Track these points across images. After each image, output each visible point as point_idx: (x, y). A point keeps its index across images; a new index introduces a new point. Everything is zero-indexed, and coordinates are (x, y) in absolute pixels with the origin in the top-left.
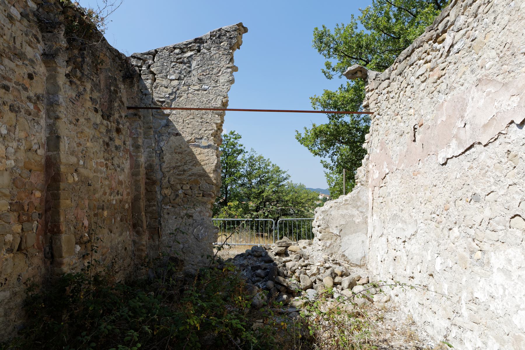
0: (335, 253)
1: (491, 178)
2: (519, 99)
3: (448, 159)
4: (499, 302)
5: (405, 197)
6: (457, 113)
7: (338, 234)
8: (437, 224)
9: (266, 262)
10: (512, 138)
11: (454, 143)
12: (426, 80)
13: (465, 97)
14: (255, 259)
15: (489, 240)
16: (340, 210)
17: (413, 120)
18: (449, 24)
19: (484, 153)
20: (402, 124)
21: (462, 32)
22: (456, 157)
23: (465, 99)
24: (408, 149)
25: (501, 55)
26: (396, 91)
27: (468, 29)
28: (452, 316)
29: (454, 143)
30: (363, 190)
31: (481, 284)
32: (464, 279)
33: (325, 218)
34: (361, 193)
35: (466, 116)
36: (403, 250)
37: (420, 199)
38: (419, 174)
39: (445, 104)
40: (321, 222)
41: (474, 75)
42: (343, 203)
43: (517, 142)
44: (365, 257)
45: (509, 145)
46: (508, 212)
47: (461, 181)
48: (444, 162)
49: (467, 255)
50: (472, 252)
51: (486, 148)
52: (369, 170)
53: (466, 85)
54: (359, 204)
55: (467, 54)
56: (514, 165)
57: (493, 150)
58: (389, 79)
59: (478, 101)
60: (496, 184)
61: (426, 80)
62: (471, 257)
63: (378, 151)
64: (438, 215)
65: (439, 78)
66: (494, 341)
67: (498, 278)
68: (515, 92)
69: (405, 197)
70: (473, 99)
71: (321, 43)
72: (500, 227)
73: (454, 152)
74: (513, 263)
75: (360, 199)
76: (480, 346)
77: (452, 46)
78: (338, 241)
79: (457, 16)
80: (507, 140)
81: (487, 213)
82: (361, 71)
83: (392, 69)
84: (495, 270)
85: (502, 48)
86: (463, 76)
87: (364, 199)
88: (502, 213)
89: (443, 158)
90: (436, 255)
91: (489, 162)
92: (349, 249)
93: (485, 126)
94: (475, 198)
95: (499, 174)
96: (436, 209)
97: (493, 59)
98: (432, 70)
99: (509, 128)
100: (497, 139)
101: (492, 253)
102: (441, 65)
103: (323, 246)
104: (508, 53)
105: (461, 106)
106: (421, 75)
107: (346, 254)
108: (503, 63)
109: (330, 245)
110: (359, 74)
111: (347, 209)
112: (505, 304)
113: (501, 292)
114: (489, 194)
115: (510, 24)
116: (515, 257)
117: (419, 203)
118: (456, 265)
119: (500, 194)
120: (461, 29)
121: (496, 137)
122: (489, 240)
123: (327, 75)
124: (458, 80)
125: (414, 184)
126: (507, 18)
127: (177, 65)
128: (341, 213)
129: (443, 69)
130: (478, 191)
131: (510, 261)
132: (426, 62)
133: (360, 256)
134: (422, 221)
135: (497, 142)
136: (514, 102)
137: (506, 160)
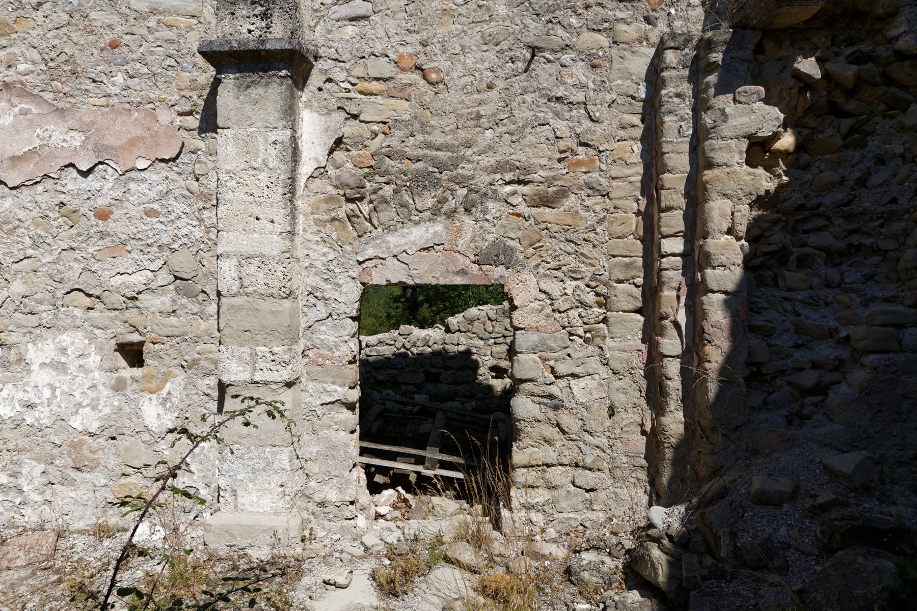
1: (27, 238)
2: (83, 138)
4: (42, 409)
25: (51, 64)
43: (78, 194)
45: (63, 196)
46: (60, 286)
51: (14, 192)
56: (71, 223)
67: (41, 377)
74: (70, 351)
80: (59, 188)
88: (49, 288)
100: (39, 182)
101: (30, 346)
108: (54, 77)
114: (21, 260)
116: (73, 343)
121: (38, 179)
122: (20, 326)
127: (561, 257)
131: (63, 351)
136: (75, 140)
137: (57, 215)
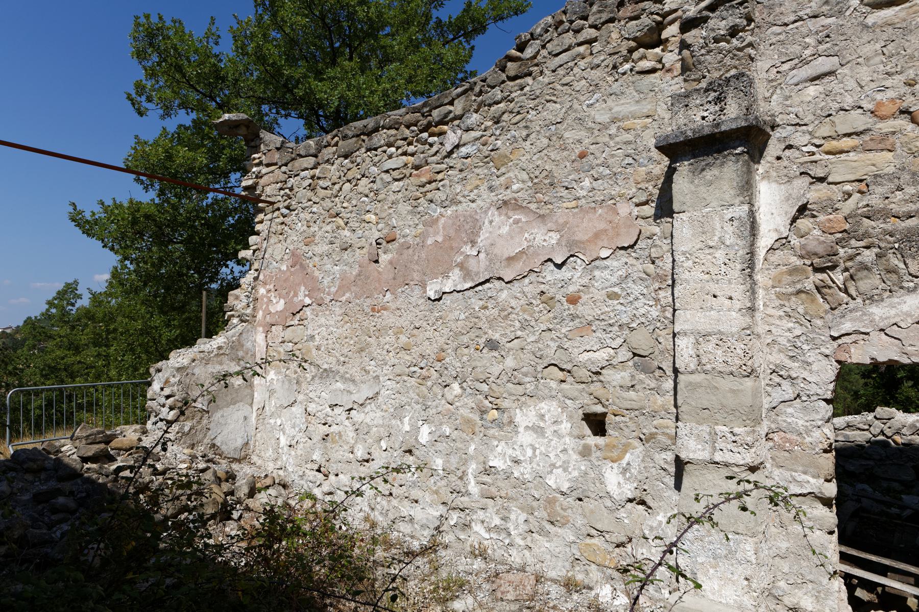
0: (198, 442)
2: (558, 236)
3: (444, 293)
5: (352, 342)
6: (463, 235)
7: (205, 408)
8: (419, 381)
9: (61, 479)
10: (548, 278)
11: (456, 274)
12: (403, 178)
13: (478, 217)
14: (29, 477)
15: (511, 394)
16: (209, 366)
17: (374, 230)
18: (451, 115)
19: (506, 291)
20: (347, 233)
21: (473, 134)
22: (458, 292)
23: (477, 220)
24: (361, 272)
25: (536, 181)
26: (334, 179)
27: (484, 133)
28: (449, 498)
29: (456, 274)
30: (248, 331)
31: (499, 449)
32: (473, 447)
33: (183, 380)
34: (244, 335)
35: (479, 240)
36: (347, 423)
37: (387, 347)
38: (385, 309)
39: (442, 220)
40: (175, 388)
41: (493, 194)
42: (215, 352)
43: (554, 284)
44: (247, 443)
45: (543, 286)
46: (540, 361)
47: (468, 323)
48: (437, 297)
49: (476, 417)
50: (483, 412)
51: (509, 285)
52: (258, 296)
53: (479, 202)
54: (241, 354)
55: (481, 164)
56: (548, 308)
57: (519, 289)
58: (316, 156)
59: (500, 227)
60: (523, 328)
61: (403, 178)
62: (482, 419)
63: (284, 268)
64: (422, 368)
65: (430, 183)
66: (519, 512)
67: (525, 438)
68: (554, 228)
69: (352, 342)
70: (491, 222)
71: (151, 45)
72: (527, 379)
73: (456, 286)
74: (547, 418)
75: (243, 346)
76: (498, 523)
77: (457, 147)
78: (205, 421)
79: (466, 111)
80: (541, 280)
81: (510, 362)
82: (248, 127)
83: (324, 143)
84: (521, 429)
85: (537, 173)
86: (476, 191)
87: (249, 345)
88: (532, 363)
89: (436, 292)
90: (421, 423)
91: (513, 303)
92: (222, 434)
93: (510, 259)
94: (492, 345)
95: (528, 318)
96: (420, 360)
97: (523, 182)
98: (417, 168)
99: (544, 267)
101: (518, 411)
102: (434, 166)
103: (178, 433)
104: (547, 181)
105: (470, 230)
106: (394, 170)
107: (218, 442)
109: (190, 430)
110: (243, 130)
111: (221, 364)
112: (535, 466)
113: (529, 452)
115: (549, 149)
116: (549, 411)
117: (385, 352)
118: (456, 432)
119: (529, 340)
120: (472, 130)
122: (511, 394)
123: (136, 106)
124: (466, 193)
125: (374, 324)
126: (546, 141)
128: (211, 370)
129: (438, 173)
130: (496, 336)
131: (542, 417)
132: (405, 154)
133: (239, 442)
134: (391, 377)
135: (527, 280)
137: (539, 302)
